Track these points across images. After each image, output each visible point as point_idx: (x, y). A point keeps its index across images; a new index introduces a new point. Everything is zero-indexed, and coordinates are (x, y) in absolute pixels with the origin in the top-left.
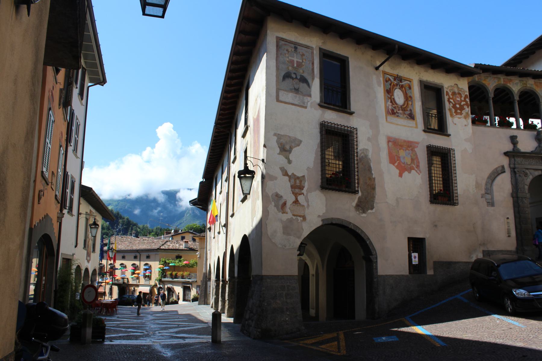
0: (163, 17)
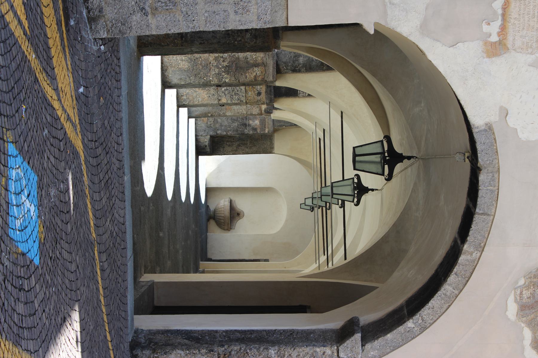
0: (354, 148)
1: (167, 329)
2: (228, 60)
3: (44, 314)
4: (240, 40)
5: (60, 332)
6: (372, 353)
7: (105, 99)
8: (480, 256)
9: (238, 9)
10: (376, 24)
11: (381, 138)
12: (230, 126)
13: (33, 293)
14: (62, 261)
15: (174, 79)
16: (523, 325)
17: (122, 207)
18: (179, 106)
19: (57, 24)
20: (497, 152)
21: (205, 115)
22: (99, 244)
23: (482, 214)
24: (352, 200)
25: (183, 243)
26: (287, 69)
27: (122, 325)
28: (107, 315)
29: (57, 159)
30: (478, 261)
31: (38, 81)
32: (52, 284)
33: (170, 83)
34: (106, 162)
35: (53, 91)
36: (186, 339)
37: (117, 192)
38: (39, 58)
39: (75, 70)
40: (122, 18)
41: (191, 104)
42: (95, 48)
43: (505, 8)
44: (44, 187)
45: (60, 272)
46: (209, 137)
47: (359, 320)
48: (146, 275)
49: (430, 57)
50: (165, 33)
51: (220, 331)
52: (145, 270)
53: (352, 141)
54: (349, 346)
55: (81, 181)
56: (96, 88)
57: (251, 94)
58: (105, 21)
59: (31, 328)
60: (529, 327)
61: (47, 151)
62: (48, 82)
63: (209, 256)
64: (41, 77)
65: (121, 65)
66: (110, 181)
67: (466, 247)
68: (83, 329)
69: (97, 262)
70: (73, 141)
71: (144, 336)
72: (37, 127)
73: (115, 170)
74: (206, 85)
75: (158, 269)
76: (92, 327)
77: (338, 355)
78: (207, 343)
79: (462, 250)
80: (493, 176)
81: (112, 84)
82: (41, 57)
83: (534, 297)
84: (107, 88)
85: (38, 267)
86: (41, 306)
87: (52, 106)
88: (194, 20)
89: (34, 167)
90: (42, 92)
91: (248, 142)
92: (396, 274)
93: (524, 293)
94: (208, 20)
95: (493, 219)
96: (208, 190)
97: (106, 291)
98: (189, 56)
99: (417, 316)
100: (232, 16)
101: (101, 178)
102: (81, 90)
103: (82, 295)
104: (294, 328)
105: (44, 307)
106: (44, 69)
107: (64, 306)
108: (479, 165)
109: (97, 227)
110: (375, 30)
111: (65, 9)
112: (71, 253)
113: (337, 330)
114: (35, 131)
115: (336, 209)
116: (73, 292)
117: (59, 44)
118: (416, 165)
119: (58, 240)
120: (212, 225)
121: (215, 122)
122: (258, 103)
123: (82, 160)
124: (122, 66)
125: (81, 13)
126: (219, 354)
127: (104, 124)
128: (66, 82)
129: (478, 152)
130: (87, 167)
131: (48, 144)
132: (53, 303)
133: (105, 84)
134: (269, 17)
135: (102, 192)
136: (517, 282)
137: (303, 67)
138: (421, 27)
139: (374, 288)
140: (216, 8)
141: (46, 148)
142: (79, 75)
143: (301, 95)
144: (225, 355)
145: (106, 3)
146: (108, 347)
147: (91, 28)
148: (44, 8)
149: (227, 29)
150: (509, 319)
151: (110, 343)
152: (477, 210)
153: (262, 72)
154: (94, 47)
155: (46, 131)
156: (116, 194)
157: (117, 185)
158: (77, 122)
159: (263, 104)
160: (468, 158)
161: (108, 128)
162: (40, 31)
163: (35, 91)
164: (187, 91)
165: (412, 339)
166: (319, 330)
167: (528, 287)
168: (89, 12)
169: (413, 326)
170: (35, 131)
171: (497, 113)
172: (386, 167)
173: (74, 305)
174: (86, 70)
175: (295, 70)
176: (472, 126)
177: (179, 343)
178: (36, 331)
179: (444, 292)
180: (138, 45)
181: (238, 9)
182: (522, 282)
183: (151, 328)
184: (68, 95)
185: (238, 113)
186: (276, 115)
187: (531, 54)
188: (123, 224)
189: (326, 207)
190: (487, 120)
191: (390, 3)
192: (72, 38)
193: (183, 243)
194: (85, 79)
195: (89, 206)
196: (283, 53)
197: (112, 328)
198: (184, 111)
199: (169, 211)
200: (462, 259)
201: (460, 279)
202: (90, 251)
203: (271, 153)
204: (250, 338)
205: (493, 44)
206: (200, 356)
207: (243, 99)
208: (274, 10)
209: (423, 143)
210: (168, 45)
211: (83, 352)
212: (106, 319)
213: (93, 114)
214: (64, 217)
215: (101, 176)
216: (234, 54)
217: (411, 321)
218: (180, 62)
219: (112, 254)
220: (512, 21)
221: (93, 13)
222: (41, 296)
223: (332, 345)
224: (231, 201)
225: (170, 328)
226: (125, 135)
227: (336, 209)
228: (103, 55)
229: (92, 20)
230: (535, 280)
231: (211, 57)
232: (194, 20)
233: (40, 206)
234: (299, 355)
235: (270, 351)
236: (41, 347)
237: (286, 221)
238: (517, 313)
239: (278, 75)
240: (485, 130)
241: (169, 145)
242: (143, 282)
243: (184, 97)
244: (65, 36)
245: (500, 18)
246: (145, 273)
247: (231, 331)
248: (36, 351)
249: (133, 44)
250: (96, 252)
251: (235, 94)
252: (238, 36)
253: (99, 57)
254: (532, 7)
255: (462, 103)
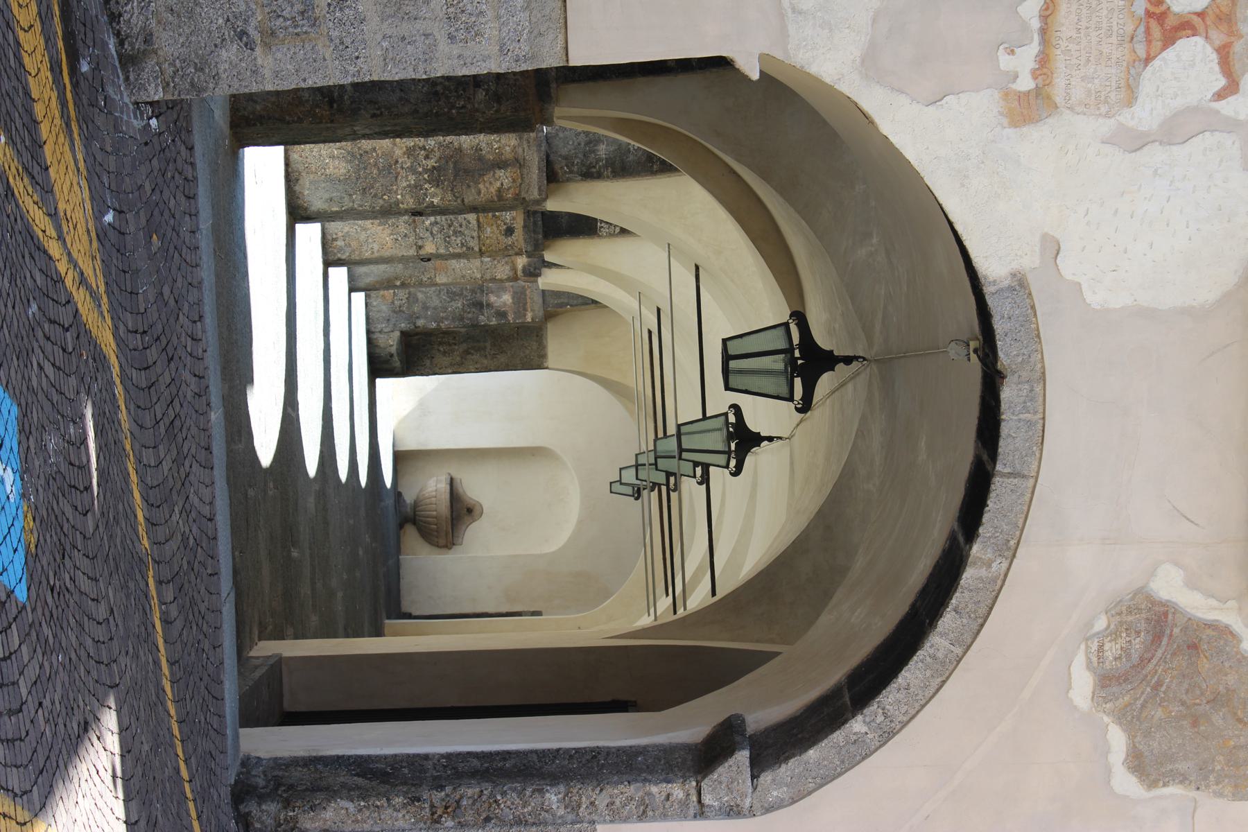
0: (724, 341)
1: (314, 754)
2: (438, 154)
3: (40, 711)
4: (463, 107)
5: (76, 753)
6: (775, 793)
7: (162, 238)
8: (1008, 569)
9: (457, 30)
10: (763, 58)
11: (785, 317)
12: (445, 309)
13: (15, 665)
14: (76, 596)
15: (316, 200)
16: (1106, 719)
17: (207, 481)
18: (328, 263)
19: (52, 69)
20: (1038, 336)
21: (388, 284)
22: (158, 563)
23: (1010, 475)
24: (724, 463)
25: (345, 577)
26: (571, 172)
27: (212, 746)
28: (180, 722)
29: (59, 369)
30: (1004, 581)
31: (13, 194)
32: (57, 645)
33: (306, 209)
34: (168, 380)
35: (47, 218)
36: (358, 775)
37: (194, 446)
38: (15, 144)
39: (94, 172)
40: (196, 54)
41: (355, 257)
42: (137, 124)
43: (1046, 17)
44: (33, 430)
45: (72, 621)
46: (397, 334)
47: (743, 721)
48: (262, 644)
49: (885, 128)
50: (293, 86)
51: (434, 755)
52: (260, 632)
53: (719, 327)
54: (723, 779)
55: (115, 421)
56: (142, 213)
57: (492, 232)
58: (157, 64)
59: (13, 740)
60: (1120, 724)
61: (38, 351)
62: (36, 198)
63: (406, 606)
64: (20, 186)
65: (198, 161)
66: (177, 423)
67: (976, 549)
68: (126, 752)
69: (155, 602)
70: (94, 332)
71: (264, 772)
72: (15, 296)
73: (189, 397)
74: (388, 212)
75: (290, 631)
76: (146, 747)
77: (699, 801)
78: (405, 783)
79: (968, 556)
80: (1031, 391)
81: (178, 204)
82: (18, 141)
83: (1129, 656)
84: (166, 213)
85: (24, 607)
86: (34, 693)
87: (45, 252)
88: (357, 58)
89: (10, 386)
90: (22, 219)
91: (488, 345)
92: (825, 619)
93: (1106, 647)
94: (391, 55)
95: (1034, 487)
96: (400, 458)
97: (175, 668)
98: (348, 145)
99: (873, 708)
100: (443, 46)
101: (159, 416)
102: (109, 218)
103: (122, 674)
104: (601, 744)
105: (41, 695)
106: (26, 169)
107: (83, 696)
108: (999, 367)
109: (153, 524)
110: (761, 72)
111: (69, 37)
112: (97, 580)
113: (696, 745)
114: (10, 305)
115: (691, 488)
116: (103, 667)
117: (57, 115)
118: (862, 379)
119: (68, 548)
120: (411, 536)
121: (412, 299)
122: (507, 252)
123: (114, 375)
124: (200, 165)
125: (104, 45)
126: (432, 806)
127: (162, 294)
128: (75, 199)
129: (997, 337)
130: (125, 389)
131: (40, 334)
132: (59, 688)
133: (161, 205)
134: (525, 48)
135: (161, 447)
136: (1090, 624)
137: (606, 167)
138: (863, 61)
139: (777, 654)
140: (405, 28)
141: (36, 345)
142: (104, 184)
143: (604, 231)
144: (446, 808)
145: (159, 22)
146: (184, 794)
147: (127, 79)
148: (21, 34)
149: (433, 75)
150: (1075, 707)
151: (187, 786)
152: (999, 467)
153: (514, 181)
154: (135, 122)
155: (34, 307)
156: (193, 451)
157: (194, 430)
158: (102, 289)
159: (519, 254)
160: (975, 351)
161: (172, 302)
162: (15, 83)
163: (8, 216)
164: (346, 229)
165: (864, 759)
166: (655, 746)
167: (1114, 635)
168: (121, 43)
169: (864, 729)
170: (10, 305)
171: (1037, 249)
172: (798, 382)
173: (106, 695)
174: (119, 174)
175: (590, 174)
176: (983, 281)
177: (343, 785)
178: (25, 748)
179: (931, 651)
180: (231, 122)
181: (457, 30)
182: (1101, 624)
183: (279, 754)
184: (81, 229)
185: (463, 277)
186: (550, 280)
187: (1107, 116)
188: (210, 520)
189: (668, 484)
190: (1015, 266)
191: (794, 10)
192: (85, 101)
193: (345, 577)
194: (117, 193)
195: (134, 477)
196: (561, 135)
197: (191, 751)
198: (339, 275)
199: (311, 502)
200: (969, 576)
201: (965, 621)
202: (138, 577)
203: (540, 367)
204: (501, 769)
205: (1023, 97)
206: (390, 811)
207: (474, 244)
208: (536, 32)
209: (878, 327)
210: (300, 120)
211: (127, 801)
212: (176, 732)
213: (138, 271)
214: (77, 498)
215: (159, 410)
216: (448, 139)
217: (859, 718)
218: (327, 159)
219: (186, 586)
220: (1063, 44)
221: (132, 44)
222: (32, 672)
223: (685, 779)
224: (452, 481)
225: (321, 754)
226: (210, 320)
227: (691, 488)
228: (155, 140)
229: (129, 61)
230: (1130, 618)
231: (397, 147)
232: (357, 58)
233: (24, 472)
234: (613, 803)
235: (548, 795)
236: (36, 783)
237: (580, 522)
238: (1093, 693)
239: (552, 185)
240: (1011, 289)
241: (306, 345)
242: (258, 658)
243: (340, 243)
244: (69, 95)
245: (1036, 37)
246: (260, 640)
247: (459, 754)
248: (25, 793)
249: (221, 117)
250: (151, 581)
251: (455, 233)
252: (459, 97)
253: (146, 144)
254: (1105, 12)
255: (958, 227)
